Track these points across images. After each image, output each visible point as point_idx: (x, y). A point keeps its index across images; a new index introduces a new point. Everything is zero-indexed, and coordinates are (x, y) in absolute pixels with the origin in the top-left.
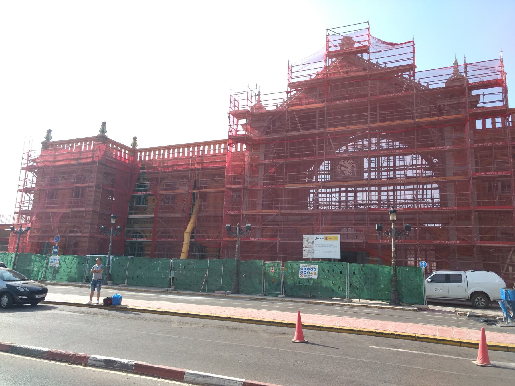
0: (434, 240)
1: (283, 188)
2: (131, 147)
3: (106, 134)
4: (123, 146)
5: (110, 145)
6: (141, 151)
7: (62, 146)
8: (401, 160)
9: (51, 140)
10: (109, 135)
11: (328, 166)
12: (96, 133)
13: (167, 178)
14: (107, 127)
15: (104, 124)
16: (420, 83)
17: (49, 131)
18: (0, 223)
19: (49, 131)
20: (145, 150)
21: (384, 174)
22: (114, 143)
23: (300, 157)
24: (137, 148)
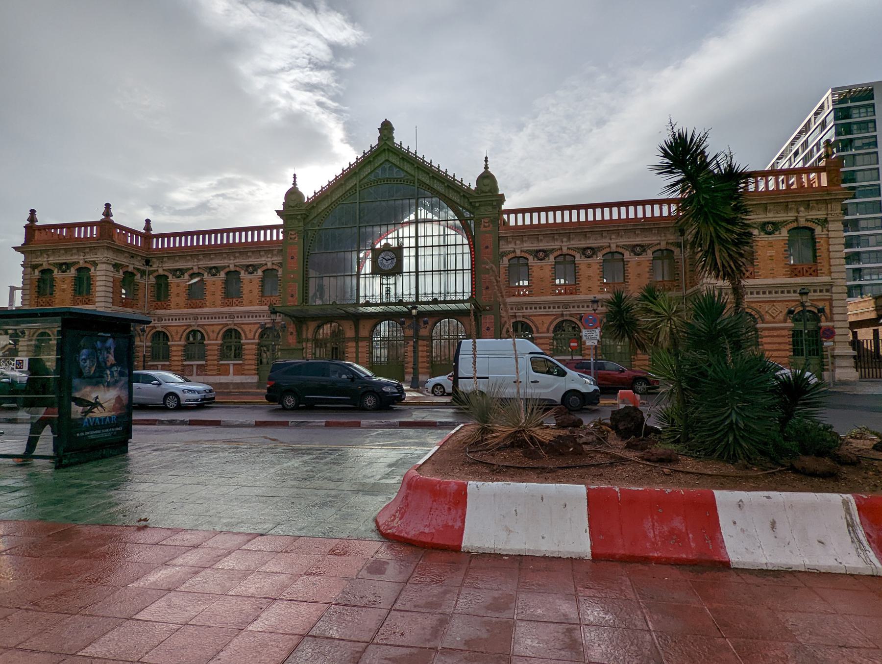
0: (509, 297)
1: (231, 367)
2: (144, 231)
3: (111, 218)
4: (133, 232)
5: (118, 231)
6: (157, 236)
7: (53, 231)
8: (429, 239)
9: (37, 224)
10: (115, 219)
11: (430, 291)
12: (99, 217)
13: (192, 268)
14: (113, 210)
15: (108, 206)
16: (504, 207)
17: (33, 212)
18: (5, 304)
19: (33, 212)
20: (163, 236)
21: (436, 239)
22: (122, 228)
23: (29, 369)
24: (152, 232)
